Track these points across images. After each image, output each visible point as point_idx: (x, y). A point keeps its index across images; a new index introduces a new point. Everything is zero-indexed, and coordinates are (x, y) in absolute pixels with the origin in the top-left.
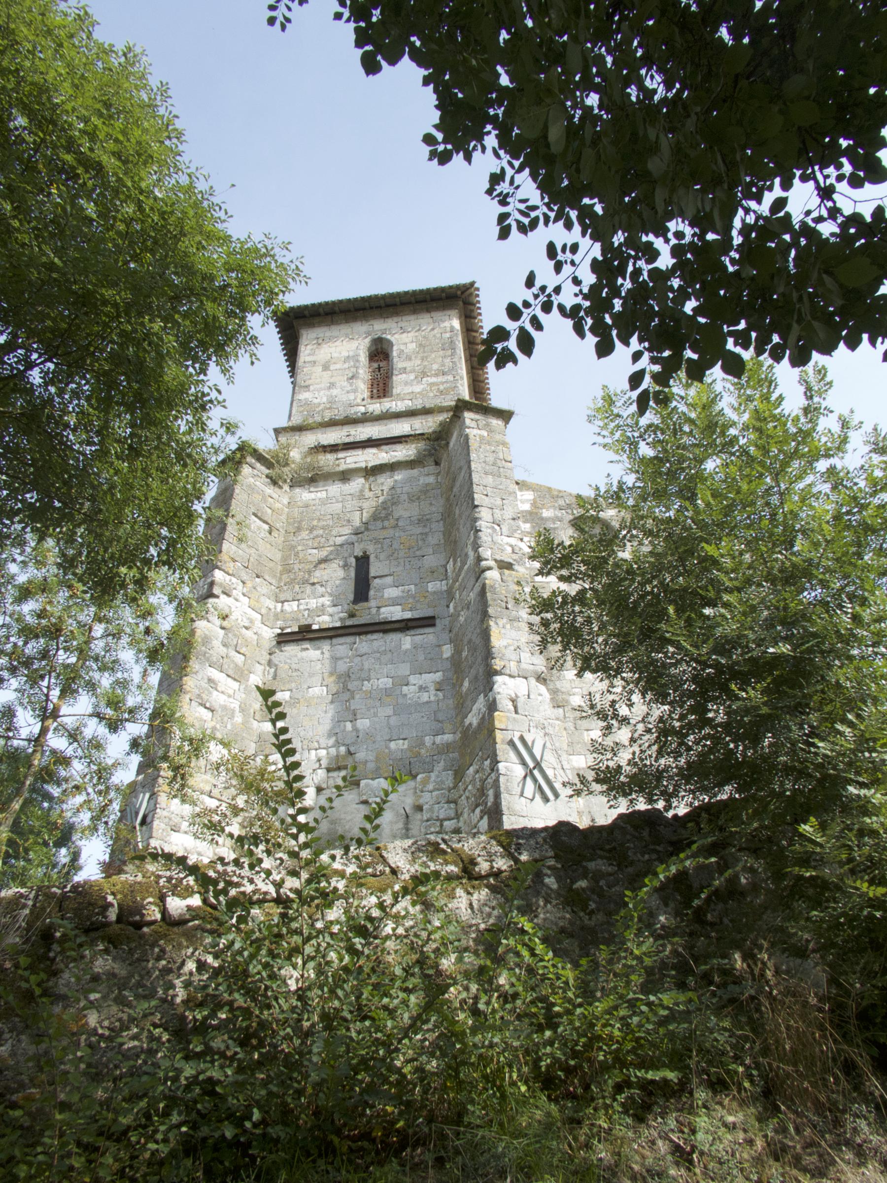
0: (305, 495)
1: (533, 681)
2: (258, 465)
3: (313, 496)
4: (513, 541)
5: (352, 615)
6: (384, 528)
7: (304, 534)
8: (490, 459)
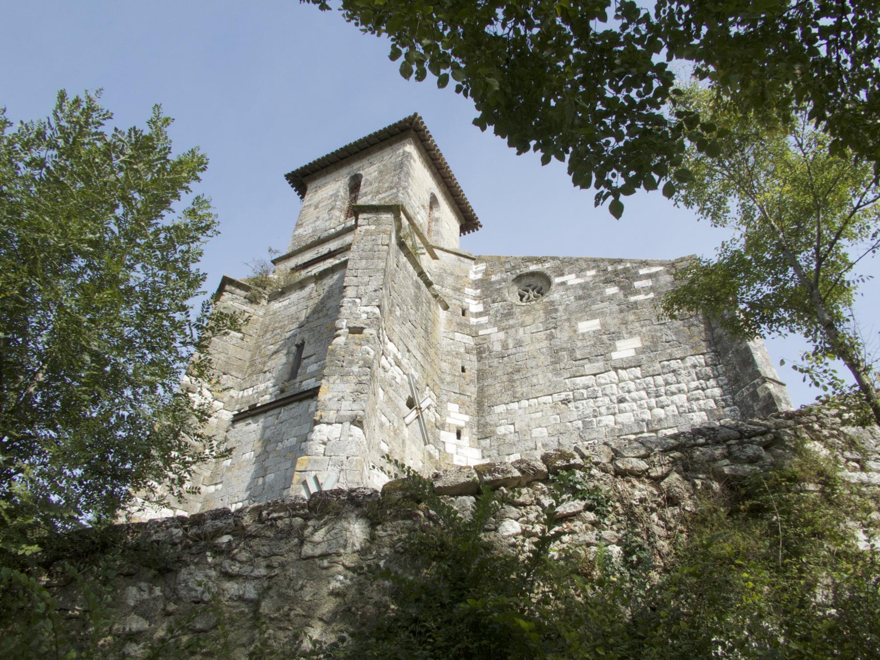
0: (276, 305)
1: (347, 424)
2: (238, 291)
3: (280, 305)
4: (368, 309)
6: (319, 318)
7: (268, 336)
8: (369, 245)
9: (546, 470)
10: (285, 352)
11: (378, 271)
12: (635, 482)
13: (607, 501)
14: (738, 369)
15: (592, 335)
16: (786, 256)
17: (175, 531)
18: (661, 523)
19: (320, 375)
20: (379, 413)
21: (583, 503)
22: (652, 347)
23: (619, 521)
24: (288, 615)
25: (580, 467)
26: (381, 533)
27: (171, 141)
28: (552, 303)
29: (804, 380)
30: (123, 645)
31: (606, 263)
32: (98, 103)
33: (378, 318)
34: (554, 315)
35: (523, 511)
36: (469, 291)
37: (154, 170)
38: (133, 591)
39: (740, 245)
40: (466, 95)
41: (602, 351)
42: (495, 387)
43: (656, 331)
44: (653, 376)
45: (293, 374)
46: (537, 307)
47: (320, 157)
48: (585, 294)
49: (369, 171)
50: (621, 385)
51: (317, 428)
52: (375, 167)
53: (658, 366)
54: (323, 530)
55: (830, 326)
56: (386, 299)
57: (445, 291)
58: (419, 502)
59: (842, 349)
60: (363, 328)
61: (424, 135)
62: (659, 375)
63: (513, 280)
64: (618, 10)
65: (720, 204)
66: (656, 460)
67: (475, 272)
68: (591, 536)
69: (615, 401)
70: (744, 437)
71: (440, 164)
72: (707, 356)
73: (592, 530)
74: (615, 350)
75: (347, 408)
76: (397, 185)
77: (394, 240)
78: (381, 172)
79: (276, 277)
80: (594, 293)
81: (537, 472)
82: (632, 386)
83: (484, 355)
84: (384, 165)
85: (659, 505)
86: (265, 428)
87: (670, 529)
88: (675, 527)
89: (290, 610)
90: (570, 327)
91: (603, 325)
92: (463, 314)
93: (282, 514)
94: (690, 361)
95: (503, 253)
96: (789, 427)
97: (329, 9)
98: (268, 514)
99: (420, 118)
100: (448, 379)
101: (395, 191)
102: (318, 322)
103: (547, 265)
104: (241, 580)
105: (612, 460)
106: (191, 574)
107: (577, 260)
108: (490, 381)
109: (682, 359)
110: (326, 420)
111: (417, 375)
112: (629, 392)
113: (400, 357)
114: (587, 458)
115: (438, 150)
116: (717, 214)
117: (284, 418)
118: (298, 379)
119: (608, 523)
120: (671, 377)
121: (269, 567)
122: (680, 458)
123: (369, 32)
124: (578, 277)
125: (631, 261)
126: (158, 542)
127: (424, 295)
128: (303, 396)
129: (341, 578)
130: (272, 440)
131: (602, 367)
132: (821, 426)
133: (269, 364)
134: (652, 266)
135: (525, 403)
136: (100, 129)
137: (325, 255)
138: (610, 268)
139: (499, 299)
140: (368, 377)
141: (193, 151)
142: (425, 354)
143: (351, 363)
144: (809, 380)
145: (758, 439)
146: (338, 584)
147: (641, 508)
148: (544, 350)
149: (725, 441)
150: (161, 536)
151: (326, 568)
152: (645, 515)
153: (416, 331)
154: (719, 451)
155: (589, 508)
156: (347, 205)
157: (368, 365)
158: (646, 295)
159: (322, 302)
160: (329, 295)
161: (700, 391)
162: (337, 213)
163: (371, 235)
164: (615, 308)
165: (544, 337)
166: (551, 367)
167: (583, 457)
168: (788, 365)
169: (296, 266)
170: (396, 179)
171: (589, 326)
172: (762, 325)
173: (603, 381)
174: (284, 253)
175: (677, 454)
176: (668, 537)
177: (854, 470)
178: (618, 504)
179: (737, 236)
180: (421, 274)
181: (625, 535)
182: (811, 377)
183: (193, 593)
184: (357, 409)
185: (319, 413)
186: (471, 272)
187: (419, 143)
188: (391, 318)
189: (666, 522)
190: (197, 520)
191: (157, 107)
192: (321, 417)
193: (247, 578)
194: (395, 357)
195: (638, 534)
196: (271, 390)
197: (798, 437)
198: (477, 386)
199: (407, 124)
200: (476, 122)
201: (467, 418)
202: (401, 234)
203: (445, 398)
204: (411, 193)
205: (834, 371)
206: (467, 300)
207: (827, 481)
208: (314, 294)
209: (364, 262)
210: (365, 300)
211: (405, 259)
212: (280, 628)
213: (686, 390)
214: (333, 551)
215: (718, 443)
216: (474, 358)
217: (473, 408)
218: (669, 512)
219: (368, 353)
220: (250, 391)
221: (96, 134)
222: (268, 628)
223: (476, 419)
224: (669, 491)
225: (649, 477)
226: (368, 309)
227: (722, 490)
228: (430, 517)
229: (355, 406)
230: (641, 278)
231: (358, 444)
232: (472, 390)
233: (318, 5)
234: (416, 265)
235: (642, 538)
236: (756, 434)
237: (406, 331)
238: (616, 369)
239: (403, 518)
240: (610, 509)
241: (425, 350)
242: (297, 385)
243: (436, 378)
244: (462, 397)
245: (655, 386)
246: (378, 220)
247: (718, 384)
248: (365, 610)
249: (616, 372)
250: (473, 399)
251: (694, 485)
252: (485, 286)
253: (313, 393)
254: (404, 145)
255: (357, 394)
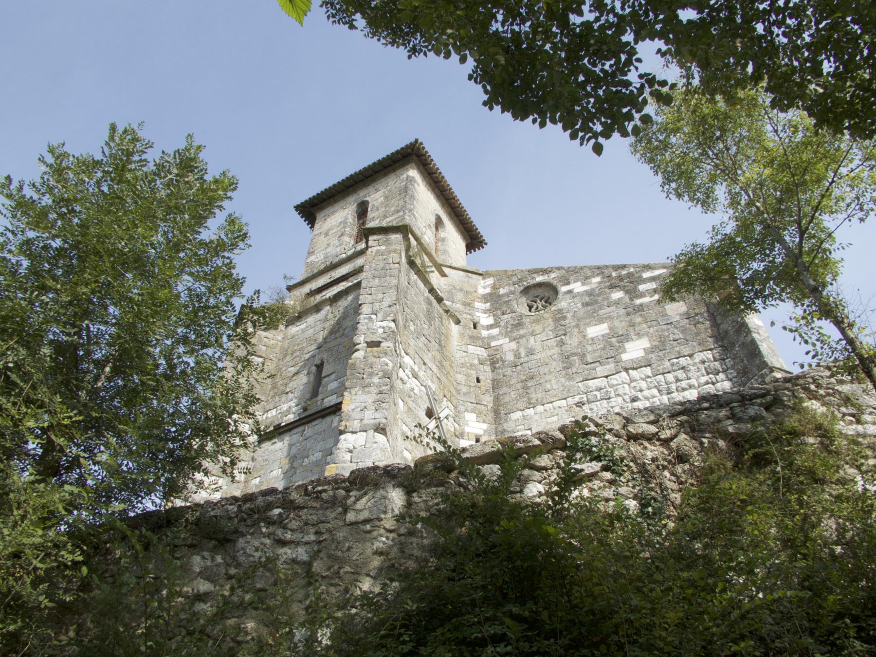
0: (293, 330)
1: (371, 432)
3: (298, 328)
4: (384, 324)
5: (305, 409)
6: (336, 338)
7: (288, 358)
9: (563, 438)
10: (305, 372)
11: (391, 287)
12: (646, 444)
13: (622, 461)
14: (745, 362)
15: (601, 339)
16: (772, 233)
17: (230, 507)
18: (673, 478)
19: (341, 390)
20: (400, 423)
21: (600, 464)
22: (660, 346)
23: (634, 479)
24: (338, 573)
25: (595, 434)
26: (417, 499)
27: (207, 163)
28: (560, 311)
29: (794, 339)
30: (193, 604)
31: (610, 270)
32: (140, 134)
33: (393, 332)
34: (563, 323)
35: (545, 474)
36: (479, 305)
37: (193, 190)
38: (197, 559)
39: (730, 228)
40: (476, 82)
41: (611, 353)
42: (510, 395)
43: (663, 331)
44: (663, 374)
45: (315, 393)
46: (546, 316)
47: (327, 187)
48: (592, 300)
49: (376, 197)
50: (633, 384)
51: (342, 437)
52: (380, 193)
53: (667, 364)
54: (364, 499)
55: (816, 291)
56: (400, 315)
57: (456, 307)
58: (450, 471)
59: (829, 311)
60: (380, 342)
61: (426, 160)
62: (669, 372)
63: (521, 292)
64: (591, 6)
65: (709, 193)
66: (665, 424)
67: (484, 287)
68: (609, 493)
69: (628, 400)
70: (745, 400)
71: (443, 186)
72: (715, 351)
73: (610, 488)
74: (625, 351)
75: (370, 417)
76: (403, 208)
77: (404, 260)
78: (386, 197)
79: (292, 303)
80: (600, 299)
81: (555, 440)
82: (643, 385)
83: (497, 365)
84: (390, 190)
85: (669, 462)
86: (291, 446)
87: (681, 483)
88: (686, 481)
89: (340, 568)
90: (579, 332)
91: (611, 329)
92: (475, 327)
93: (326, 487)
94: (699, 357)
95: (509, 267)
96: (787, 389)
97: (356, 28)
98: (314, 488)
99: (421, 143)
100: (464, 389)
101: (401, 213)
102: (335, 342)
103: (553, 275)
104: (293, 545)
105: (624, 427)
106: (248, 542)
107: (582, 268)
108: (505, 389)
109: (691, 356)
110: (351, 430)
111: (434, 387)
112: (641, 391)
113: (416, 369)
114: (601, 425)
115: (440, 173)
116: (707, 202)
117: (308, 435)
118: (320, 397)
119: (623, 480)
120: (681, 374)
121: (317, 533)
122: (687, 421)
123: (390, 45)
124: (583, 284)
125: (634, 266)
126: (216, 517)
127: (435, 311)
128: (325, 412)
129: (384, 539)
130: (298, 456)
131: (613, 369)
132: (817, 387)
133: (290, 385)
134: (655, 269)
135: (540, 408)
136: (144, 157)
137: (338, 279)
138: (614, 274)
139: (509, 311)
140: (388, 387)
141: (224, 174)
142: (441, 366)
143: (371, 375)
144: (798, 339)
145: (759, 401)
146: (381, 545)
147: (653, 466)
148: (556, 356)
149: (728, 404)
150: (217, 512)
151: (369, 532)
152: (657, 472)
153: (430, 345)
154: (723, 413)
155: (605, 468)
156: (355, 231)
157: (387, 375)
158: (651, 297)
159: (339, 323)
160: (345, 316)
161: (710, 385)
162: (346, 239)
163: (382, 255)
164: (622, 311)
165: (555, 344)
166: (563, 372)
167: (597, 425)
168: (778, 326)
169: (311, 292)
170: (401, 203)
171: (596, 331)
172: (756, 301)
173: (615, 382)
174: (298, 281)
175: (684, 418)
176: (680, 490)
177: (851, 423)
178: (632, 464)
179: (726, 219)
180: (432, 290)
181: (640, 490)
182: (801, 336)
183: (251, 559)
184: (380, 418)
185: (343, 423)
186: (479, 287)
187: (421, 167)
188: (406, 332)
189: (678, 477)
190: (249, 498)
191: (190, 136)
192: (346, 426)
193: (297, 544)
194: (412, 370)
195: (652, 489)
196: (294, 410)
197: (796, 397)
198: (493, 395)
199: (409, 150)
200: (485, 104)
201: (485, 426)
202: (411, 253)
203: (462, 408)
204: (417, 215)
205: (820, 328)
206: (477, 314)
207: (825, 433)
208: (330, 316)
209: (377, 280)
210: (380, 316)
211: (415, 277)
212: (332, 585)
213: (696, 385)
214: (375, 516)
215: (721, 406)
216: (488, 369)
217: (491, 415)
218: (679, 469)
219: (387, 365)
220: (274, 412)
221: (141, 161)
222: (320, 585)
223: (493, 427)
224: (678, 449)
225: (659, 440)
226: (384, 324)
227: (728, 447)
228: (460, 485)
229: (378, 415)
230: (645, 281)
231: (383, 450)
232: (488, 400)
233: (347, 26)
234: (426, 282)
235: (656, 492)
236: (757, 396)
237: (421, 345)
238: (626, 370)
239: (436, 486)
240: (625, 468)
241: (440, 362)
242: (319, 403)
243: (452, 389)
244: (479, 406)
245: (666, 383)
246: (387, 240)
247: (727, 377)
248: (407, 565)
249: (627, 372)
250: (489, 408)
251: (702, 443)
252: (494, 300)
253: (336, 408)
254: (407, 170)
255: (379, 404)
